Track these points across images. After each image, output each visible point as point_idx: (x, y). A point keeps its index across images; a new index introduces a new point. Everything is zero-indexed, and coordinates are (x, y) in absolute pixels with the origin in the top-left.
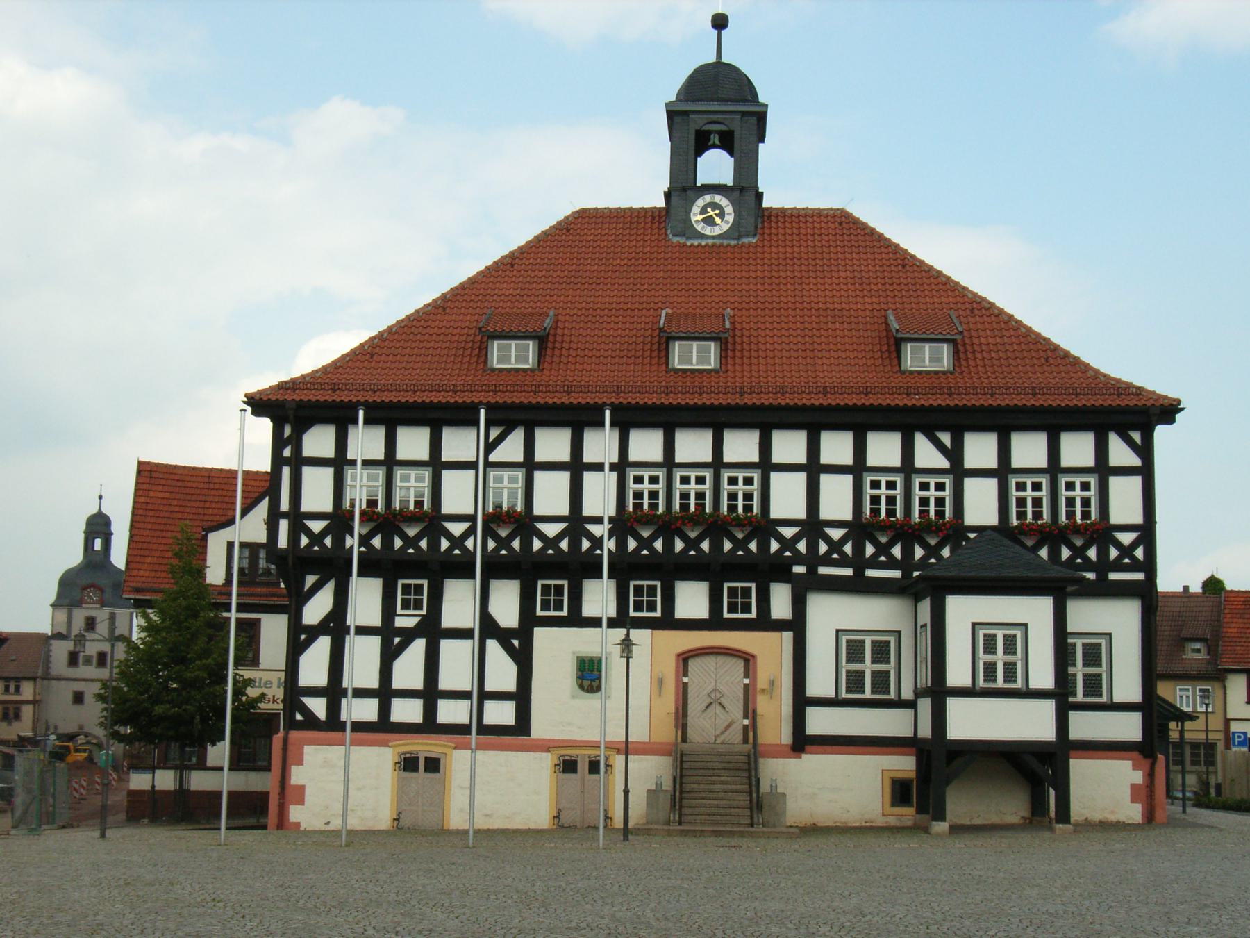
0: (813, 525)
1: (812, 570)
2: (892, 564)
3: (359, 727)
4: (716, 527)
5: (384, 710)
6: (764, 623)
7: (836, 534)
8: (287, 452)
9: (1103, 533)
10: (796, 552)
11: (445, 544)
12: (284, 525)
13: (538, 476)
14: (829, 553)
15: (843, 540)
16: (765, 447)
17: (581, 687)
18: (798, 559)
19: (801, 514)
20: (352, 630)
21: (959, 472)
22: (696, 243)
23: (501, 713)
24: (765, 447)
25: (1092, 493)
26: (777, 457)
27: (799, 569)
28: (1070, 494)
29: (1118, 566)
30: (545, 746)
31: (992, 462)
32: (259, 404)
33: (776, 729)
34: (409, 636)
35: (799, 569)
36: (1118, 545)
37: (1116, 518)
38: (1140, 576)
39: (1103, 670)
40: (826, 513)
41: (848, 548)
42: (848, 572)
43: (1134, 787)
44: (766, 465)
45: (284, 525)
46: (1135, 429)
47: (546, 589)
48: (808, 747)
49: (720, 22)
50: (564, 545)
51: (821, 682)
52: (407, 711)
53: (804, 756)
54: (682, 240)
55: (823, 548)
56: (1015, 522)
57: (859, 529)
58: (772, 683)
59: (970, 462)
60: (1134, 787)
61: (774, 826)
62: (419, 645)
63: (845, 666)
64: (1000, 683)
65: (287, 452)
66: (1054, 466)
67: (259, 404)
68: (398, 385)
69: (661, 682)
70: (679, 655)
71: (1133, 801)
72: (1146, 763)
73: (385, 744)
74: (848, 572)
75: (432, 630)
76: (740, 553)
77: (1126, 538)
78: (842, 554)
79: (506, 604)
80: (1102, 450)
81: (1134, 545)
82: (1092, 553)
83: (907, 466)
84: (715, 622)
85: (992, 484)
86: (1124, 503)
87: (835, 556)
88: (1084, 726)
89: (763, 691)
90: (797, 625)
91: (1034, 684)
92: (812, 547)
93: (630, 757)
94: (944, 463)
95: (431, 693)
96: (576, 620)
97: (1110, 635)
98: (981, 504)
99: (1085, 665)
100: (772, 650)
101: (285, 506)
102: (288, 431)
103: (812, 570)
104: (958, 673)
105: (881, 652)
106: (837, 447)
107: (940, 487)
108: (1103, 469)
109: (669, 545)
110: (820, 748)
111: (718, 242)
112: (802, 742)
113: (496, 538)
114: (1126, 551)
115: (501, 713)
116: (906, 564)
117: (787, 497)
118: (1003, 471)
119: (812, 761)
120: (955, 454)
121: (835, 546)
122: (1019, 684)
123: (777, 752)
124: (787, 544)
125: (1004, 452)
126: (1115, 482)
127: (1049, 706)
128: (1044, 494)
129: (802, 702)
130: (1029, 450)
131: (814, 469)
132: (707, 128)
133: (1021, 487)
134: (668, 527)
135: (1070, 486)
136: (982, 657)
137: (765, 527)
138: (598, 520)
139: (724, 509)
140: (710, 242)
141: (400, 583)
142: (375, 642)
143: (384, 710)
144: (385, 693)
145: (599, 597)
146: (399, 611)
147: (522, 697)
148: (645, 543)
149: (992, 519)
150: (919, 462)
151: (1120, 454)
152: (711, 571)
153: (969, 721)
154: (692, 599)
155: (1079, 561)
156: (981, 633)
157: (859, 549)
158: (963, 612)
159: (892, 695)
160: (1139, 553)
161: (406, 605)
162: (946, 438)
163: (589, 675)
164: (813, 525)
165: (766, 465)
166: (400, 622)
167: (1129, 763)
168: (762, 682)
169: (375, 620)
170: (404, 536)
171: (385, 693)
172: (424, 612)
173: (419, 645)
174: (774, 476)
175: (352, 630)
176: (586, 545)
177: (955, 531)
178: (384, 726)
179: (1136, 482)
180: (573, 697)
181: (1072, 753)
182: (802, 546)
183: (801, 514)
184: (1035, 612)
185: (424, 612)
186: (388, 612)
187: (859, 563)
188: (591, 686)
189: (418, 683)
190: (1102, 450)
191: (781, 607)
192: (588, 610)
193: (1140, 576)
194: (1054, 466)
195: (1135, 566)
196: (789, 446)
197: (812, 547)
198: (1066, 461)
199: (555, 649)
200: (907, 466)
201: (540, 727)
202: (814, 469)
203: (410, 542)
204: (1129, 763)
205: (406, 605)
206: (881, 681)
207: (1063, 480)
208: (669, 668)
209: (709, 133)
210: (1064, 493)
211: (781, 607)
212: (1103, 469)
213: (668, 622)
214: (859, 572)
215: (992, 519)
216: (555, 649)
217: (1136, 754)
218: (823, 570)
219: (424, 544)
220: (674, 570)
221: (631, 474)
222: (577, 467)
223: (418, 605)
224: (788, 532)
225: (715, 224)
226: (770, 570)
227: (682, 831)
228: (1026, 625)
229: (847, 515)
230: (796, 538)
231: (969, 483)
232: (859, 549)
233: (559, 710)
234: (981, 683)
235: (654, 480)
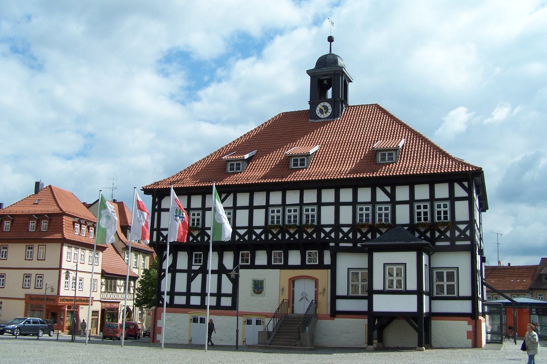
0: (337, 226)
1: (337, 245)
2: (349, 241)
3: (226, 308)
4: (301, 229)
5: (188, 300)
6: (321, 266)
7: (327, 230)
8: (157, 207)
9: (453, 224)
10: (330, 237)
11: (254, 237)
12: (155, 233)
13: (238, 212)
14: (343, 238)
15: (349, 232)
16: (319, 197)
17: (261, 292)
18: (331, 240)
19: (332, 222)
20: (210, 272)
21: (394, 203)
22: (317, 121)
23: (226, 302)
24: (319, 197)
25: (448, 209)
26: (324, 200)
27: (332, 244)
28: (419, 210)
29: (459, 239)
30: (243, 314)
31: (407, 198)
32: (147, 191)
33: (324, 308)
34: (196, 273)
35: (332, 244)
36: (459, 230)
37: (458, 218)
38: (468, 243)
39: (455, 283)
40: (342, 222)
41: (350, 235)
42: (351, 245)
43: (468, 332)
44: (319, 204)
45: (155, 233)
46: (387, 185)
47: (196, 255)
48: (337, 316)
49: (331, 39)
50: (246, 237)
51: (341, 290)
52: (195, 301)
53: (336, 319)
54: (313, 121)
55: (341, 235)
56: (416, 222)
57: (354, 227)
58: (324, 290)
59: (398, 199)
60: (468, 332)
61: (305, 346)
62: (200, 276)
63: (455, 283)
64: (395, 288)
65: (157, 207)
66: (432, 198)
67: (147, 191)
68: (189, 183)
69: (283, 290)
70: (290, 279)
71: (468, 338)
72: (473, 322)
73: (187, 313)
74: (351, 245)
75: (204, 271)
76: (463, 236)
77: (462, 227)
78: (348, 238)
79: (229, 261)
80: (451, 191)
81: (466, 229)
82: (448, 234)
83: (374, 201)
84: (303, 266)
85: (350, 208)
86: (461, 211)
87: (364, 239)
88: (441, 306)
89: (321, 293)
90: (333, 267)
91: (409, 288)
92: (337, 235)
93: (239, 317)
94: (388, 199)
95: (203, 294)
96: (253, 266)
97: (348, 269)
98: (403, 215)
99: (447, 281)
100: (324, 275)
101: (155, 227)
102: (157, 200)
103: (337, 245)
104: (378, 285)
105: (451, 277)
106: (346, 195)
107: (386, 209)
108: (452, 199)
109: (283, 236)
110: (355, 316)
111: (326, 120)
112: (334, 313)
113: (193, 236)
114: (463, 232)
115: (226, 302)
116: (354, 241)
117: (327, 216)
118: (354, 203)
119: (339, 321)
120: (392, 196)
121: (346, 235)
122: (403, 288)
123: (324, 318)
124: (328, 234)
125: (412, 193)
126: (457, 204)
127: (414, 297)
128: (428, 210)
129: (334, 297)
130: (422, 192)
131: (337, 204)
132: (322, 78)
133: (419, 207)
134: (283, 229)
135: (307, 210)
136: (388, 278)
137: (319, 228)
138: (209, 229)
139: (304, 222)
140: (323, 120)
141: (194, 253)
142: (185, 275)
143: (188, 300)
144: (188, 294)
145: (261, 258)
146: (193, 264)
147: (234, 295)
148: (275, 236)
149: (407, 221)
150: (378, 199)
151: (459, 192)
152: (303, 247)
153: (383, 304)
154: (294, 258)
155: (463, 236)
156: (387, 268)
157: (355, 235)
158: (380, 258)
159: (456, 295)
160: (468, 233)
161: (196, 262)
162: (388, 189)
163: (258, 287)
164: (337, 226)
165: (319, 204)
166: (194, 268)
167: (466, 322)
168: (320, 290)
169: (185, 267)
170: (307, 233)
171: (188, 294)
172: (202, 264)
173: (200, 276)
174: (238, 211)
175: (210, 272)
176: (206, 238)
177: (393, 226)
178: (188, 306)
179: (466, 203)
180: (252, 296)
181: (432, 318)
182: (333, 235)
183: (332, 222)
184: (409, 258)
185: (202, 264)
186: (190, 264)
187: (354, 241)
188: (258, 291)
189: (199, 290)
190: (451, 191)
191: (327, 260)
192: (257, 262)
193: (468, 243)
194: (432, 198)
195: (466, 238)
196: (328, 196)
197: (337, 235)
198: (437, 196)
199: (247, 277)
200: (374, 201)
201: (241, 307)
202: (337, 204)
203: (275, 236)
204: (466, 322)
205: (196, 262)
206: (451, 289)
207: (436, 204)
208: (286, 284)
209: (323, 80)
210: (436, 209)
211: (327, 260)
212: (452, 199)
213: (286, 266)
214: (453, 243)
215: (407, 221)
216: (247, 277)
217: (469, 318)
218: (341, 245)
219: (314, 236)
220: (287, 247)
221: (270, 209)
222: (251, 208)
223: (200, 262)
224: (327, 230)
225: (323, 114)
226: (321, 246)
227: (265, 347)
228: (405, 264)
229: (350, 222)
230: (331, 232)
231: (398, 207)
232: (355, 235)
233: (247, 301)
234: (387, 288)
235: (425, 207)
